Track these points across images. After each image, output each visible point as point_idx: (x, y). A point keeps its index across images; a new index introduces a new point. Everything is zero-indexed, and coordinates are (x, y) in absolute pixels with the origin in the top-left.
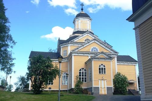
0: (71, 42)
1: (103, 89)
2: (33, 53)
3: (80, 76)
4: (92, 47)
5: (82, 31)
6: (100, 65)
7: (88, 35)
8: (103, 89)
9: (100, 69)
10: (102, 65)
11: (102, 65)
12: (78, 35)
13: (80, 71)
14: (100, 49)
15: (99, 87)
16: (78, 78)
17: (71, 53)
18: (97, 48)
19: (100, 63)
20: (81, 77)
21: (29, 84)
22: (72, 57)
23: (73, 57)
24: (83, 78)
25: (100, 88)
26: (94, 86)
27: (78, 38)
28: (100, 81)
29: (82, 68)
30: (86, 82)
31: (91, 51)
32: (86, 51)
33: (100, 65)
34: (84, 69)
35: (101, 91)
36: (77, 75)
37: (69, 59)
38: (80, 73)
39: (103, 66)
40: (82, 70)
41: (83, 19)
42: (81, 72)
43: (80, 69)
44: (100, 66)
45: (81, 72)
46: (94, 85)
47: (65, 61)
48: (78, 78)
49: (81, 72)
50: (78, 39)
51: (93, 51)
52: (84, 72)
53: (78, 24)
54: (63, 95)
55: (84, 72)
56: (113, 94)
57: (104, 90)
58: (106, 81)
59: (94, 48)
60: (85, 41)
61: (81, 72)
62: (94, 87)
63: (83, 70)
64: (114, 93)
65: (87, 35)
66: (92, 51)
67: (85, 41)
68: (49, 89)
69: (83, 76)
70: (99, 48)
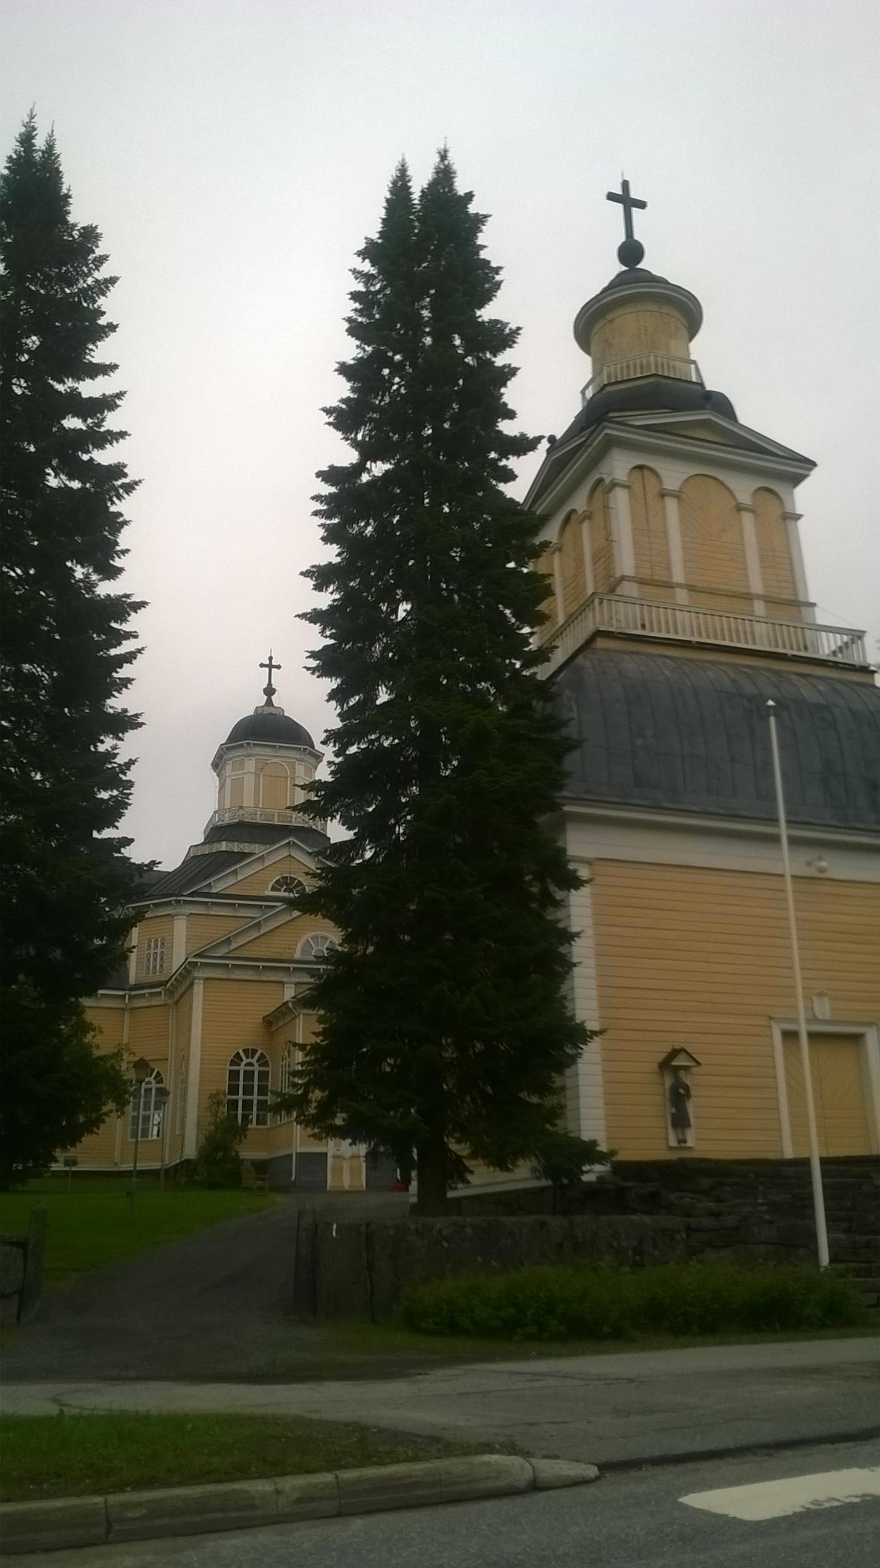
0: (192, 894)
1: (346, 1165)
2: (516, 477)
3: (233, 1089)
7: (296, 854)
8: (346, 1165)
13: (232, 1063)
15: (326, 1154)
16: (219, 1103)
17: (189, 968)
20: (241, 1097)
21: (456, 1189)
22: (192, 984)
23: (199, 988)
24: (248, 1105)
25: (330, 1160)
27: (235, 872)
29: (246, 1051)
30: (265, 1123)
31: (297, 956)
34: (254, 1051)
35: (338, 1171)
37: (177, 996)
38: (234, 1075)
40: (245, 1061)
41: (268, 751)
42: (242, 1068)
43: (238, 1055)
47: (156, 1001)
48: (219, 1103)
50: (232, 880)
52: (257, 1068)
55: (257, 1068)
56: (79, 1160)
57: (352, 1170)
60: (273, 889)
62: (301, 1156)
63: (254, 1061)
65: (285, 853)
67: (273, 889)
68: (66, 1164)
69: (248, 1090)
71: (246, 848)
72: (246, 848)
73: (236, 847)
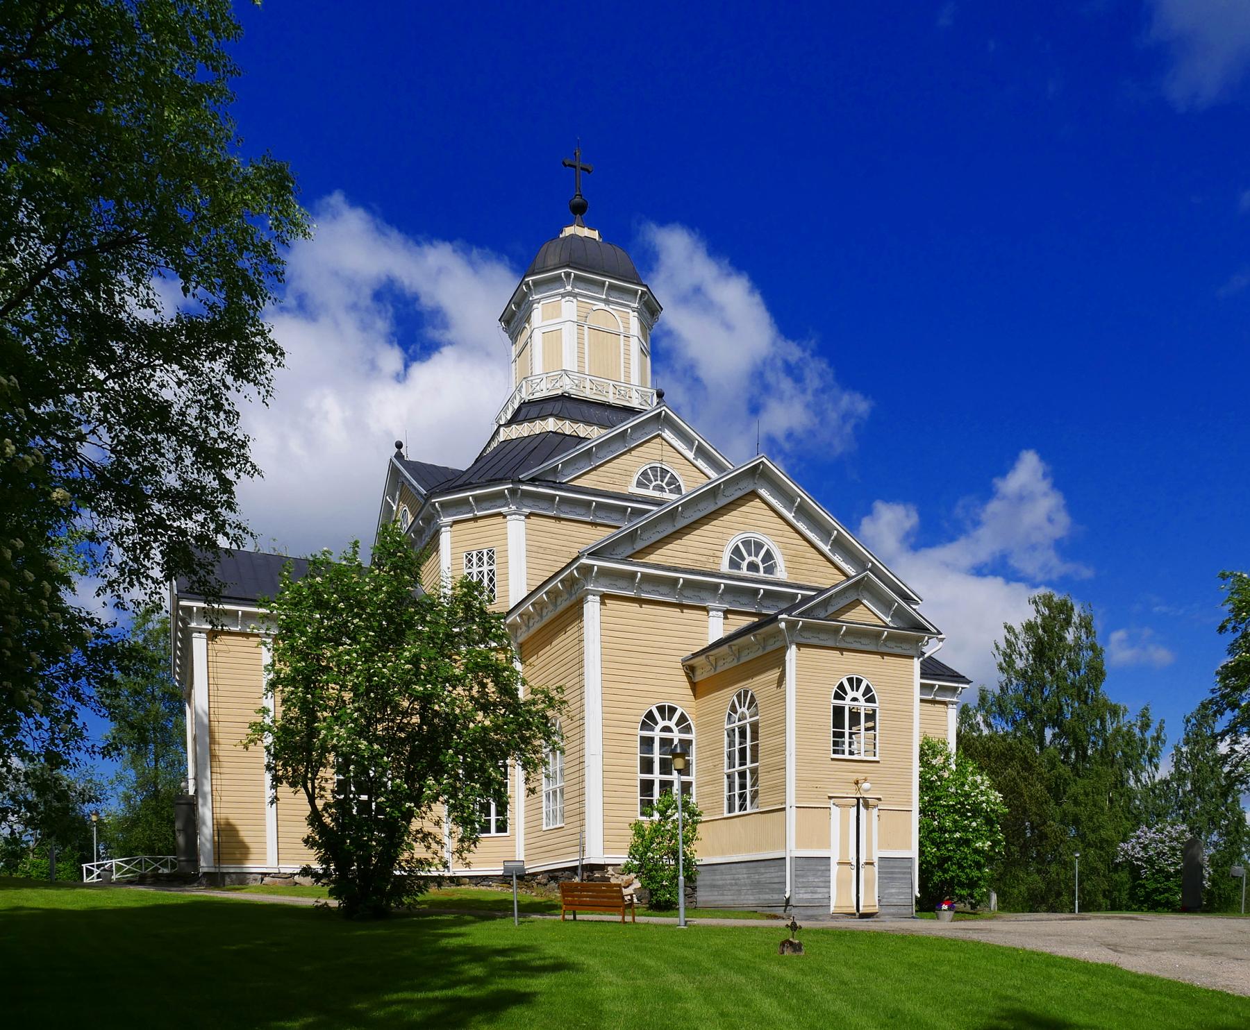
0: (532, 481)
4: (736, 540)
5: (589, 394)
6: (841, 686)
9: (838, 712)
10: (855, 683)
11: (855, 683)
12: (567, 428)
13: (644, 726)
14: (792, 560)
18: (769, 543)
19: (272, 708)
26: (793, 850)
28: (836, 811)
29: (661, 709)
32: (689, 564)
33: (841, 686)
36: (268, 777)
38: (647, 743)
39: (859, 694)
40: (662, 723)
42: (657, 734)
44: (840, 694)
45: (652, 739)
46: (799, 845)
49: (652, 739)
51: (744, 572)
53: (553, 337)
54: (797, 948)
58: (875, 811)
59: (746, 543)
61: (657, 734)
64: (928, 903)
66: (735, 572)
70: (784, 546)
71: (582, 430)
72: (582, 430)
73: (567, 428)
